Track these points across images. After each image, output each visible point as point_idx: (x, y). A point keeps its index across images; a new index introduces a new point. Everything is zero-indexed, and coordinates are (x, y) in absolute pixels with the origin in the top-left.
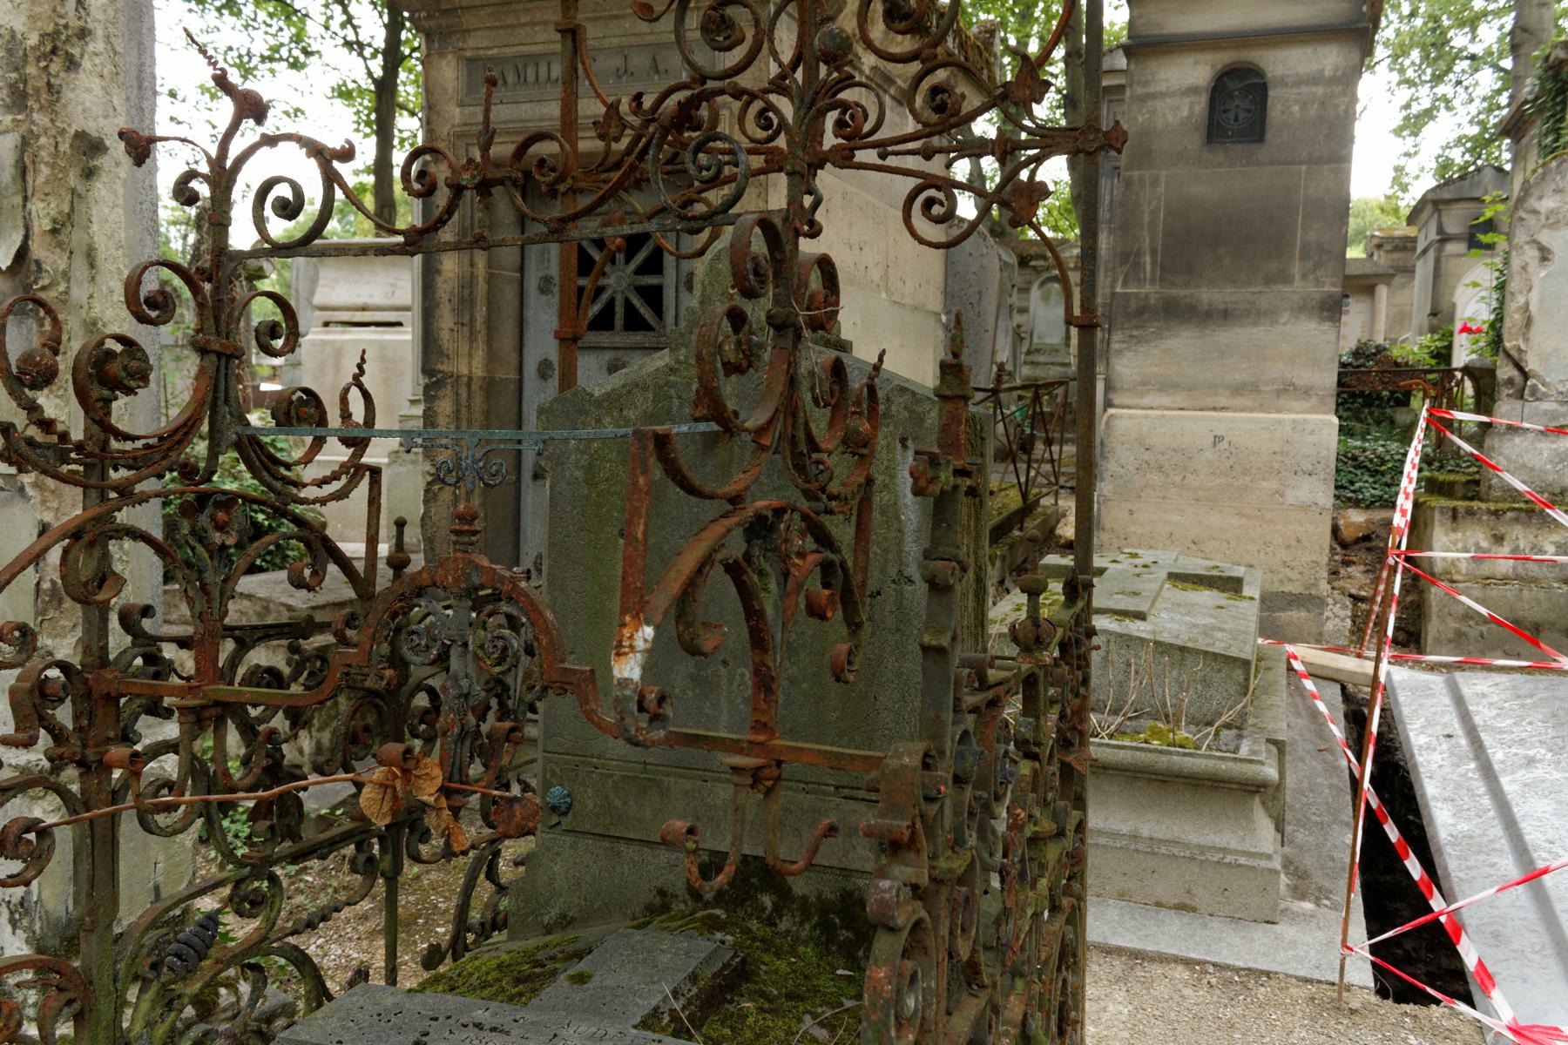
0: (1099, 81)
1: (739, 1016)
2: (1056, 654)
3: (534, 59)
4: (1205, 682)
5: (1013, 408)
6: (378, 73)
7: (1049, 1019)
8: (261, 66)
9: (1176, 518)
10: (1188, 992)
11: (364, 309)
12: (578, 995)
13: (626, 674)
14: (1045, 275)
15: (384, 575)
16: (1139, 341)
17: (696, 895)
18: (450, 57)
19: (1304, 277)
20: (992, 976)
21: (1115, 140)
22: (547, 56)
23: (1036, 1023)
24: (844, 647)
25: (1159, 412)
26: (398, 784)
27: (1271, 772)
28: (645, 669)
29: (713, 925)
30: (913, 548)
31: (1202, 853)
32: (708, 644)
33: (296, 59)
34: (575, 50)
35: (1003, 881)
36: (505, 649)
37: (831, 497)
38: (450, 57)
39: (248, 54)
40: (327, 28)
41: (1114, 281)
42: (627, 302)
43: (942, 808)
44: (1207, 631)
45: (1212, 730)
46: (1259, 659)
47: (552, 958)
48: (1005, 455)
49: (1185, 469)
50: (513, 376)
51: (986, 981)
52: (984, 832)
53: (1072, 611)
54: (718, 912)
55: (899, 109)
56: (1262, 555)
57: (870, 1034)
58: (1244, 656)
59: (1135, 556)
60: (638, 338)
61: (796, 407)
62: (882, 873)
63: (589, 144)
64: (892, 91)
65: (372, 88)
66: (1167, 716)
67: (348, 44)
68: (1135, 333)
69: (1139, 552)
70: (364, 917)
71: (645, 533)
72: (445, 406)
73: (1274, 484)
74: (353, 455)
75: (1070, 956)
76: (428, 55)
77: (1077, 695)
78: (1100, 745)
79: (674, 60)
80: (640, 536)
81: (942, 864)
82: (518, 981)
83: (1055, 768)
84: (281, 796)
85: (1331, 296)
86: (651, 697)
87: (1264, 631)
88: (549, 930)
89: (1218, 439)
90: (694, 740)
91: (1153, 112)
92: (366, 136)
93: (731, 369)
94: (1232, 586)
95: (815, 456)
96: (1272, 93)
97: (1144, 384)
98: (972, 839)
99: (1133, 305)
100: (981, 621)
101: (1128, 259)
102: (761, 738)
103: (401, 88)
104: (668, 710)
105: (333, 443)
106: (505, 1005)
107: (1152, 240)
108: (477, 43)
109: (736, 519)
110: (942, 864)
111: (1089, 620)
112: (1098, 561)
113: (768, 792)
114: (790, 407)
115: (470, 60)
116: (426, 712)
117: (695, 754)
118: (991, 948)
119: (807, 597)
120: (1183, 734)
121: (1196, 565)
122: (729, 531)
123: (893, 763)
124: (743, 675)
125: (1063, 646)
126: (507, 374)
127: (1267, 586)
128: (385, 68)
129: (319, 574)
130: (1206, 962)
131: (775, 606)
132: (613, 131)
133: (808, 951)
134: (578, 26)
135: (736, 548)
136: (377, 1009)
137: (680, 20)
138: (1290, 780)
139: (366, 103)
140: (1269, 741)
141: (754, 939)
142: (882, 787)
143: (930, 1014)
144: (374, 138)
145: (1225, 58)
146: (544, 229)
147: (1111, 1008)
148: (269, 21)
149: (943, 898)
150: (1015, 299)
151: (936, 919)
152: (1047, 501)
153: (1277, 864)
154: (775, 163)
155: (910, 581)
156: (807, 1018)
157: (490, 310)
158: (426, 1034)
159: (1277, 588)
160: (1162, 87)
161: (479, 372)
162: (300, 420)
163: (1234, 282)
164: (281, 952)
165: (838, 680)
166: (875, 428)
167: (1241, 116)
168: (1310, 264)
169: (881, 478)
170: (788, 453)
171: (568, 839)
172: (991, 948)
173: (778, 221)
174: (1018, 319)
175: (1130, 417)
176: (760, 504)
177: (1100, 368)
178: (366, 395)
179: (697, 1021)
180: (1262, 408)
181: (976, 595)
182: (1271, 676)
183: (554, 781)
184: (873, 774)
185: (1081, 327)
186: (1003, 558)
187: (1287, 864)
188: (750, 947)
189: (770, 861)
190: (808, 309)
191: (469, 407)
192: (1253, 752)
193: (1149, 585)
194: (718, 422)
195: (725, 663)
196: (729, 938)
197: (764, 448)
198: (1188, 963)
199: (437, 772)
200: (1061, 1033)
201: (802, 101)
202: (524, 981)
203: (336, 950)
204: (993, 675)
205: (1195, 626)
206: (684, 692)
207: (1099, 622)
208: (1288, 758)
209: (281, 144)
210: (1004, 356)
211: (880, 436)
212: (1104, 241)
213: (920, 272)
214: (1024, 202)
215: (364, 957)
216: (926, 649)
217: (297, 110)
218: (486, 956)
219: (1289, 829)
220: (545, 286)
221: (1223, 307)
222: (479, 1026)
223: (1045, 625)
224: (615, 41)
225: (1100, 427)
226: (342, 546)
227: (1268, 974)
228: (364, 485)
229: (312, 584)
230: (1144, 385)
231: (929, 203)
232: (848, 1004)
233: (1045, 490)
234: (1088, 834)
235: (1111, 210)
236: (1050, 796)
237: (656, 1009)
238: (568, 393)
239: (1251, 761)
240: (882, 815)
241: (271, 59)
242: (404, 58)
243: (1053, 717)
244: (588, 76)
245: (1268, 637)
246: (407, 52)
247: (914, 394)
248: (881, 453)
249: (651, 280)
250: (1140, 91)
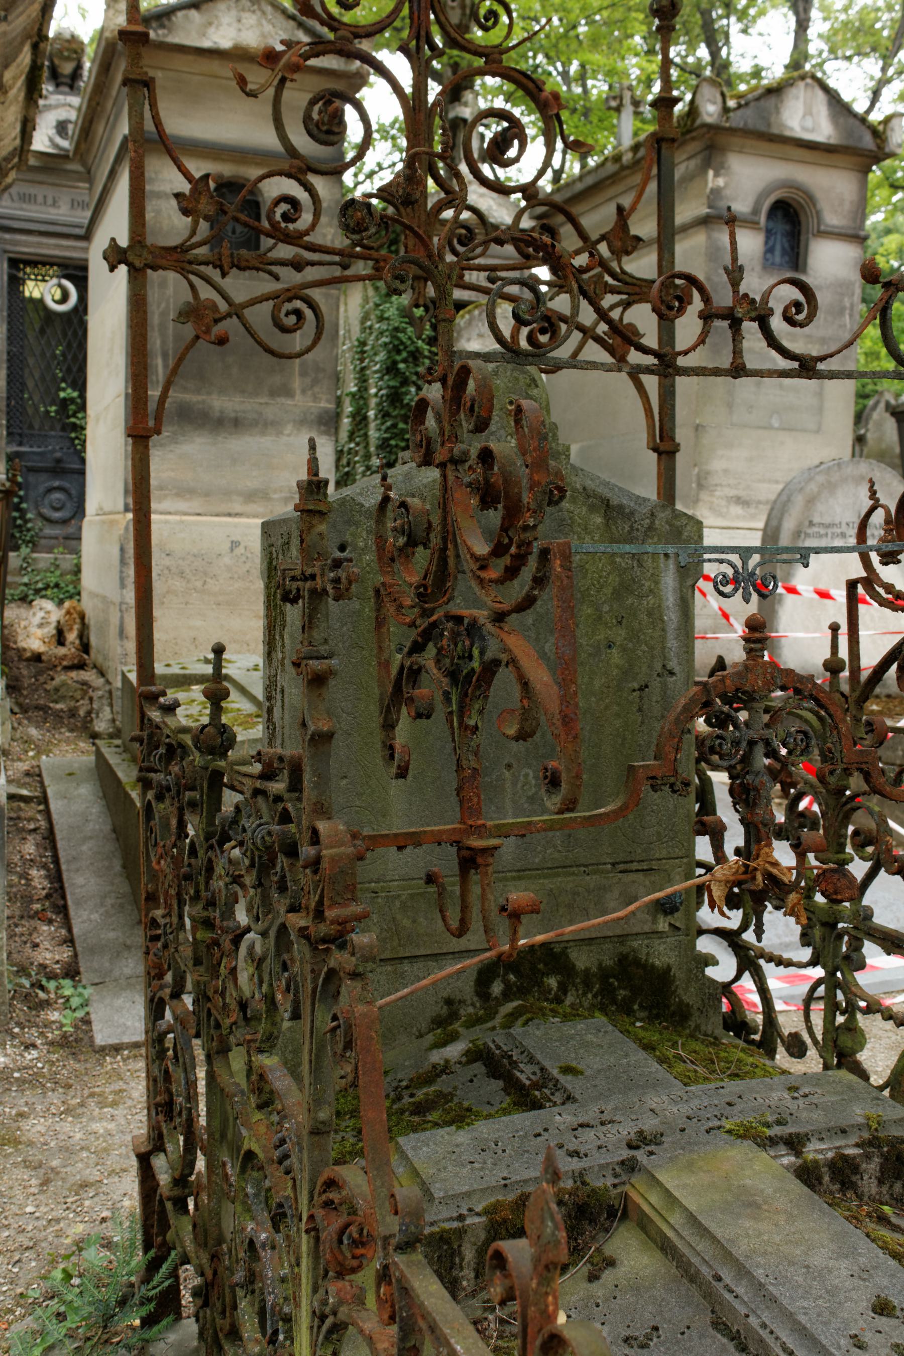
19: (304, 392)
25: (177, 518)
49: (205, 573)
85: (327, 411)
89: (235, 545)
107: (163, 343)
124: (526, 775)
155: (672, 673)
163: (243, 392)
168: (308, 380)
169: (647, 584)
195: (509, 766)
221: (233, 415)
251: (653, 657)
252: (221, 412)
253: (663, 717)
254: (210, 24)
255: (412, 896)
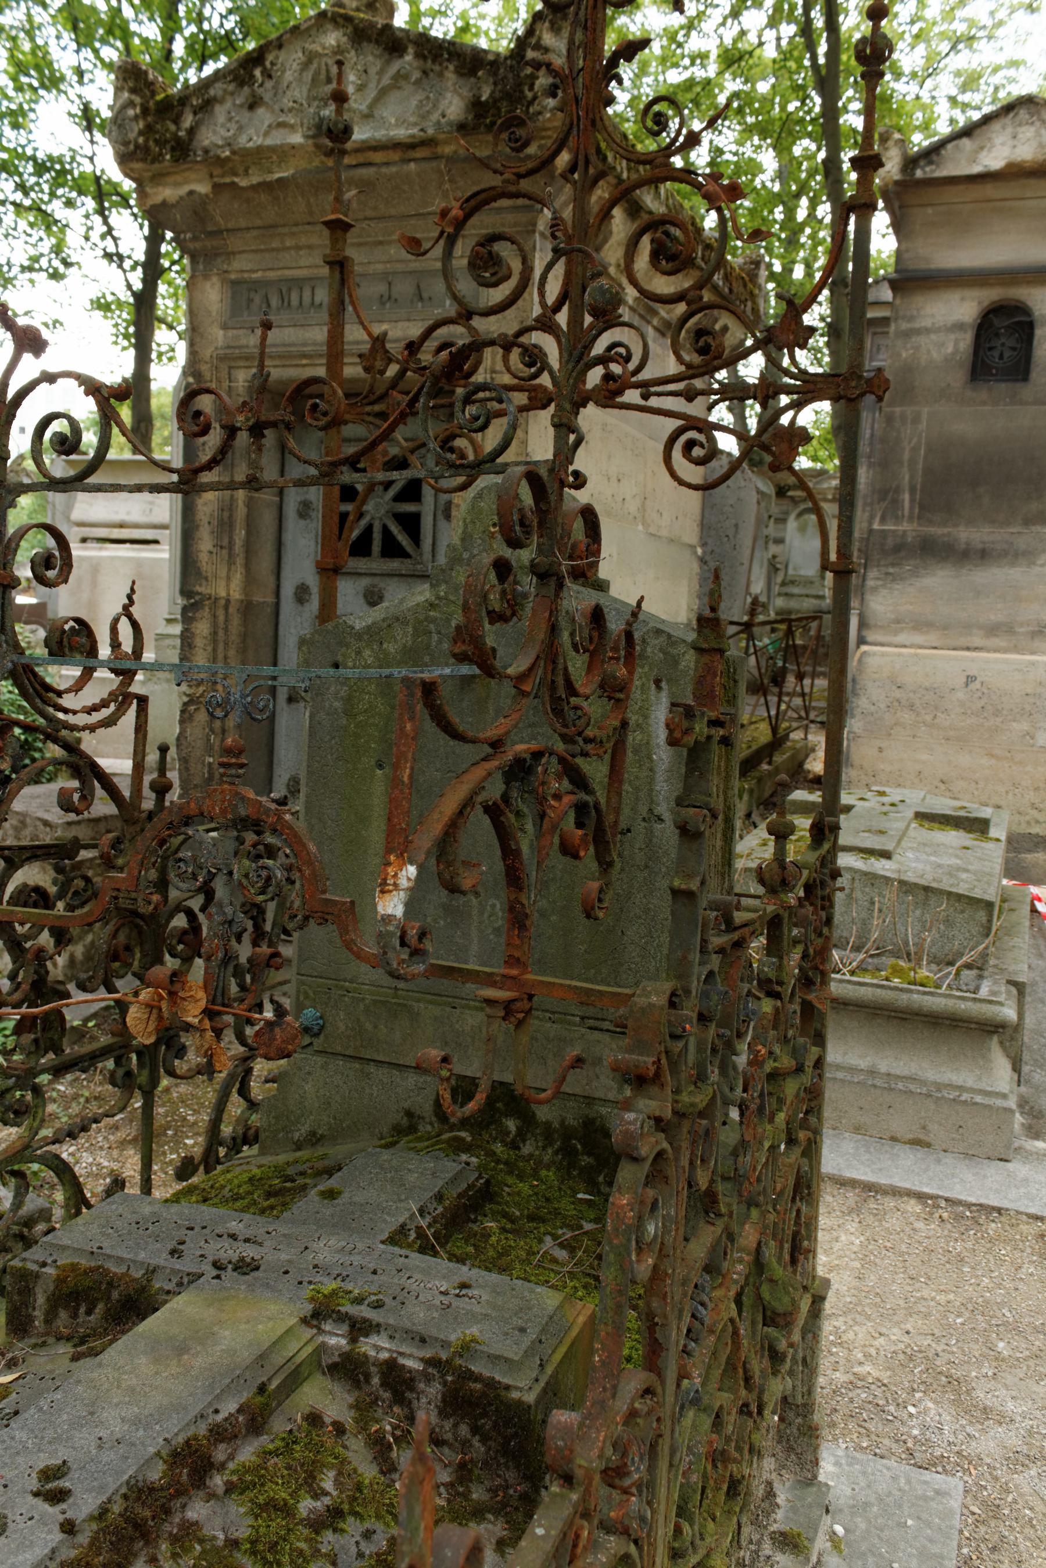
0: (864, 313)
1: (483, 1235)
2: (802, 894)
3: (298, 283)
4: (948, 922)
5: (766, 641)
6: (138, 286)
7: (782, 1248)
8: (20, 276)
9: (924, 757)
10: (920, 1225)
11: (121, 526)
12: (328, 1210)
13: (390, 911)
14: (802, 506)
15: (148, 803)
16: (895, 578)
17: (442, 1116)
18: (215, 279)
20: (729, 1205)
21: (877, 386)
22: (312, 281)
23: (770, 1252)
24: (595, 885)
26: (164, 1005)
27: (1010, 1013)
28: (408, 905)
29: (458, 1147)
30: (665, 788)
31: (939, 1090)
32: (467, 884)
33: (56, 269)
34: (343, 282)
35: (742, 1115)
36: (269, 879)
37: (588, 741)
38: (215, 279)
39: (8, 264)
40: (87, 239)
41: (872, 518)
42: (385, 529)
43: (686, 1046)
44: (952, 872)
45: (953, 970)
46: (1004, 900)
47: (302, 1174)
48: (758, 688)
49: (936, 708)
50: (271, 599)
51: (723, 1210)
52: (726, 1067)
53: (817, 854)
54: (463, 1134)
55: (661, 340)
56: (1010, 796)
57: (612, 1256)
58: (987, 897)
59: (882, 794)
60: (395, 564)
61: (556, 654)
62: (627, 1105)
63: (352, 370)
64: (655, 322)
65: (131, 300)
66: (908, 954)
67: (108, 256)
68: (891, 570)
69: (887, 790)
70: (116, 1127)
71: (411, 776)
72: (202, 628)
73: (1025, 726)
74: (122, 683)
75: (805, 1187)
76: (192, 277)
77: (820, 935)
78: (841, 981)
79: (439, 286)
80: (406, 779)
81: (685, 1098)
82: (269, 1195)
83: (796, 1007)
84: (46, 1013)
86: (413, 933)
87: (1010, 871)
88: (299, 1147)
89: (970, 679)
90: (449, 972)
91: (917, 348)
92: (124, 349)
93: (496, 617)
94: (979, 826)
95: (573, 700)
96: (1038, 332)
97: (898, 621)
98: (714, 1075)
99: (890, 542)
100: (728, 856)
101: (887, 496)
102: (514, 972)
103: (159, 301)
104: (428, 945)
105: (102, 673)
106: (258, 1218)
107: (912, 478)
108: (241, 265)
109: (496, 763)
110: (685, 1098)
111: (834, 860)
112: (845, 799)
113: (520, 1024)
114: (550, 654)
115: (234, 283)
116: (185, 932)
117: (445, 984)
118: (728, 1179)
119: (562, 838)
120: (924, 973)
121: (943, 805)
122: (489, 774)
123: (641, 1001)
124: (493, 906)
125: (808, 888)
126: (263, 597)
127: (1015, 828)
128: (144, 281)
129: (87, 797)
130: (938, 1197)
131: (531, 846)
132: (379, 364)
133: (550, 1175)
134: (347, 258)
135: (495, 790)
136: (135, 1218)
137: (448, 254)
138: (1029, 1020)
139: (125, 315)
140: (1009, 982)
141: (498, 1162)
142: (630, 1023)
143: (669, 1240)
144: (132, 352)
145: (991, 295)
146: (313, 471)
147: (843, 1238)
148: (29, 230)
149: (685, 1130)
150: (771, 530)
151: (677, 1150)
152: (796, 736)
153: (1012, 1103)
154: (539, 400)
155: (660, 819)
156: (548, 1239)
157: (249, 533)
158: (183, 1243)
159: (1024, 829)
160: (927, 323)
161: (236, 595)
162: (71, 649)
163: (993, 522)
164: (43, 1160)
165: (588, 916)
166: (631, 673)
167: (1007, 354)
170: (547, 698)
171: (320, 1060)
172: (728, 1179)
173: (543, 472)
174: (774, 549)
175: (883, 655)
176: (520, 747)
177: (854, 603)
178: (135, 625)
179: (443, 1239)
180: (1016, 649)
181: (724, 835)
182: (1014, 917)
183: (307, 1003)
184: (622, 1011)
185: (837, 573)
186: (751, 791)
187: (1023, 1103)
188: (494, 1169)
189: (519, 1090)
190: (571, 558)
191: (226, 630)
192: (993, 993)
193: (896, 824)
194: (480, 667)
196: (474, 1160)
197: (524, 694)
198: (921, 1197)
199: (201, 994)
200: (794, 1261)
201: (570, 355)
202: (276, 1195)
203: (87, 1158)
204: (739, 917)
205: (940, 866)
206: (435, 921)
207: (844, 860)
208: (1028, 999)
209: (60, 381)
210: (758, 587)
211: (636, 676)
212: (863, 475)
213: (679, 510)
214: (784, 446)
215: (115, 1166)
216: (675, 893)
217: (56, 322)
218: (238, 1170)
219: (1026, 1069)
220: (304, 511)
221: (980, 546)
222: (233, 1237)
223: (791, 868)
224: (380, 267)
225: (853, 663)
226: (103, 762)
227: (999, 1210)
228: (130, 715)
229: (81, 807)
230: (898, 623)
231: (690, 445)
232: (588, 1226)
233: (795, 724)
234: (827, 1068)
235: (871, 444)
236: (790, 1033)
237: (403, 1226)
238: (329, 626)
239: (990, 1002)
240: (629, 1050)
241: (30, 269)
242: (163, 271)
243: (796, 955)
244: (353, 303)
245: (1013, 878)
246: (166, 264)
247: (669, 636)
248: (636, 694)
249: (410, 508)
250: (904, 326)
251: (637, 799)
252: (968, 544)
253: (647, 867)
254: (982, 148)
255: (375, 1002)
